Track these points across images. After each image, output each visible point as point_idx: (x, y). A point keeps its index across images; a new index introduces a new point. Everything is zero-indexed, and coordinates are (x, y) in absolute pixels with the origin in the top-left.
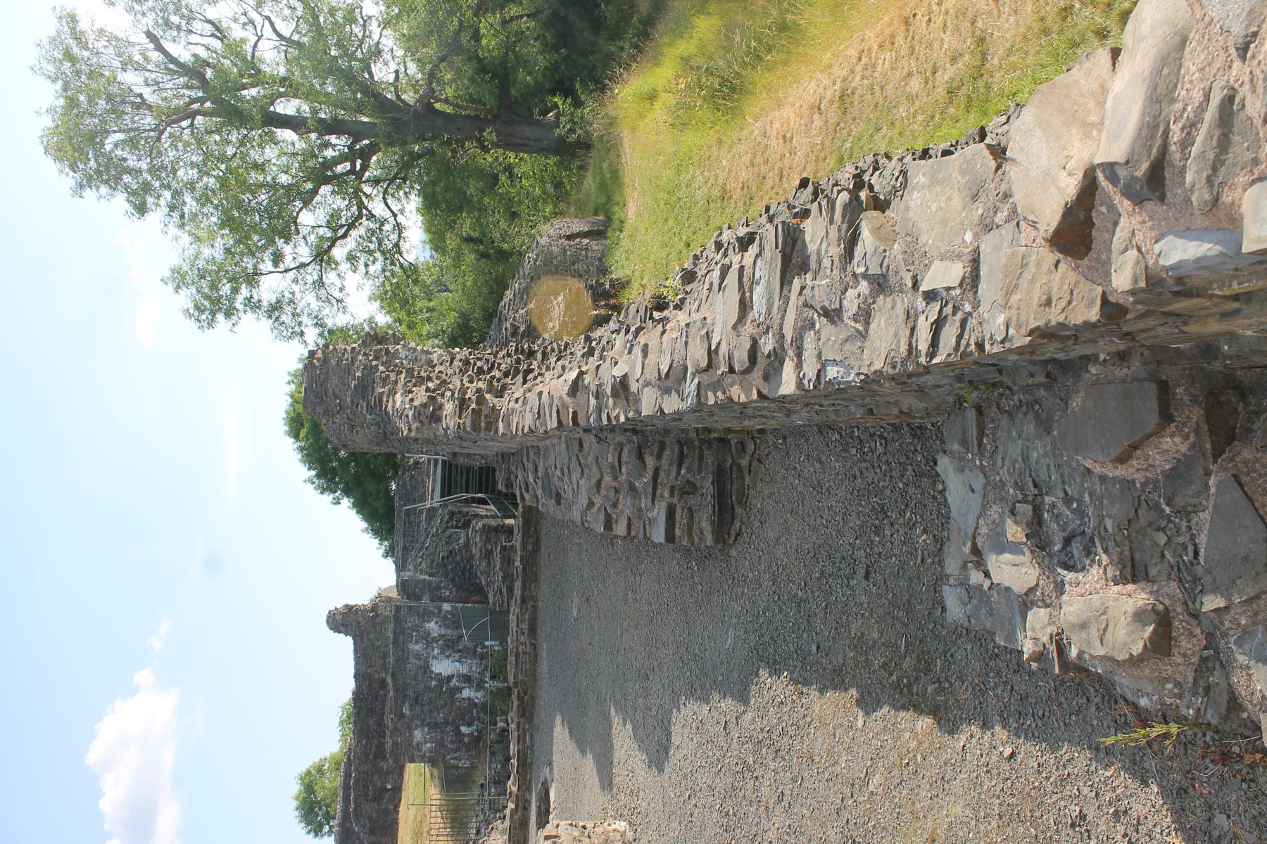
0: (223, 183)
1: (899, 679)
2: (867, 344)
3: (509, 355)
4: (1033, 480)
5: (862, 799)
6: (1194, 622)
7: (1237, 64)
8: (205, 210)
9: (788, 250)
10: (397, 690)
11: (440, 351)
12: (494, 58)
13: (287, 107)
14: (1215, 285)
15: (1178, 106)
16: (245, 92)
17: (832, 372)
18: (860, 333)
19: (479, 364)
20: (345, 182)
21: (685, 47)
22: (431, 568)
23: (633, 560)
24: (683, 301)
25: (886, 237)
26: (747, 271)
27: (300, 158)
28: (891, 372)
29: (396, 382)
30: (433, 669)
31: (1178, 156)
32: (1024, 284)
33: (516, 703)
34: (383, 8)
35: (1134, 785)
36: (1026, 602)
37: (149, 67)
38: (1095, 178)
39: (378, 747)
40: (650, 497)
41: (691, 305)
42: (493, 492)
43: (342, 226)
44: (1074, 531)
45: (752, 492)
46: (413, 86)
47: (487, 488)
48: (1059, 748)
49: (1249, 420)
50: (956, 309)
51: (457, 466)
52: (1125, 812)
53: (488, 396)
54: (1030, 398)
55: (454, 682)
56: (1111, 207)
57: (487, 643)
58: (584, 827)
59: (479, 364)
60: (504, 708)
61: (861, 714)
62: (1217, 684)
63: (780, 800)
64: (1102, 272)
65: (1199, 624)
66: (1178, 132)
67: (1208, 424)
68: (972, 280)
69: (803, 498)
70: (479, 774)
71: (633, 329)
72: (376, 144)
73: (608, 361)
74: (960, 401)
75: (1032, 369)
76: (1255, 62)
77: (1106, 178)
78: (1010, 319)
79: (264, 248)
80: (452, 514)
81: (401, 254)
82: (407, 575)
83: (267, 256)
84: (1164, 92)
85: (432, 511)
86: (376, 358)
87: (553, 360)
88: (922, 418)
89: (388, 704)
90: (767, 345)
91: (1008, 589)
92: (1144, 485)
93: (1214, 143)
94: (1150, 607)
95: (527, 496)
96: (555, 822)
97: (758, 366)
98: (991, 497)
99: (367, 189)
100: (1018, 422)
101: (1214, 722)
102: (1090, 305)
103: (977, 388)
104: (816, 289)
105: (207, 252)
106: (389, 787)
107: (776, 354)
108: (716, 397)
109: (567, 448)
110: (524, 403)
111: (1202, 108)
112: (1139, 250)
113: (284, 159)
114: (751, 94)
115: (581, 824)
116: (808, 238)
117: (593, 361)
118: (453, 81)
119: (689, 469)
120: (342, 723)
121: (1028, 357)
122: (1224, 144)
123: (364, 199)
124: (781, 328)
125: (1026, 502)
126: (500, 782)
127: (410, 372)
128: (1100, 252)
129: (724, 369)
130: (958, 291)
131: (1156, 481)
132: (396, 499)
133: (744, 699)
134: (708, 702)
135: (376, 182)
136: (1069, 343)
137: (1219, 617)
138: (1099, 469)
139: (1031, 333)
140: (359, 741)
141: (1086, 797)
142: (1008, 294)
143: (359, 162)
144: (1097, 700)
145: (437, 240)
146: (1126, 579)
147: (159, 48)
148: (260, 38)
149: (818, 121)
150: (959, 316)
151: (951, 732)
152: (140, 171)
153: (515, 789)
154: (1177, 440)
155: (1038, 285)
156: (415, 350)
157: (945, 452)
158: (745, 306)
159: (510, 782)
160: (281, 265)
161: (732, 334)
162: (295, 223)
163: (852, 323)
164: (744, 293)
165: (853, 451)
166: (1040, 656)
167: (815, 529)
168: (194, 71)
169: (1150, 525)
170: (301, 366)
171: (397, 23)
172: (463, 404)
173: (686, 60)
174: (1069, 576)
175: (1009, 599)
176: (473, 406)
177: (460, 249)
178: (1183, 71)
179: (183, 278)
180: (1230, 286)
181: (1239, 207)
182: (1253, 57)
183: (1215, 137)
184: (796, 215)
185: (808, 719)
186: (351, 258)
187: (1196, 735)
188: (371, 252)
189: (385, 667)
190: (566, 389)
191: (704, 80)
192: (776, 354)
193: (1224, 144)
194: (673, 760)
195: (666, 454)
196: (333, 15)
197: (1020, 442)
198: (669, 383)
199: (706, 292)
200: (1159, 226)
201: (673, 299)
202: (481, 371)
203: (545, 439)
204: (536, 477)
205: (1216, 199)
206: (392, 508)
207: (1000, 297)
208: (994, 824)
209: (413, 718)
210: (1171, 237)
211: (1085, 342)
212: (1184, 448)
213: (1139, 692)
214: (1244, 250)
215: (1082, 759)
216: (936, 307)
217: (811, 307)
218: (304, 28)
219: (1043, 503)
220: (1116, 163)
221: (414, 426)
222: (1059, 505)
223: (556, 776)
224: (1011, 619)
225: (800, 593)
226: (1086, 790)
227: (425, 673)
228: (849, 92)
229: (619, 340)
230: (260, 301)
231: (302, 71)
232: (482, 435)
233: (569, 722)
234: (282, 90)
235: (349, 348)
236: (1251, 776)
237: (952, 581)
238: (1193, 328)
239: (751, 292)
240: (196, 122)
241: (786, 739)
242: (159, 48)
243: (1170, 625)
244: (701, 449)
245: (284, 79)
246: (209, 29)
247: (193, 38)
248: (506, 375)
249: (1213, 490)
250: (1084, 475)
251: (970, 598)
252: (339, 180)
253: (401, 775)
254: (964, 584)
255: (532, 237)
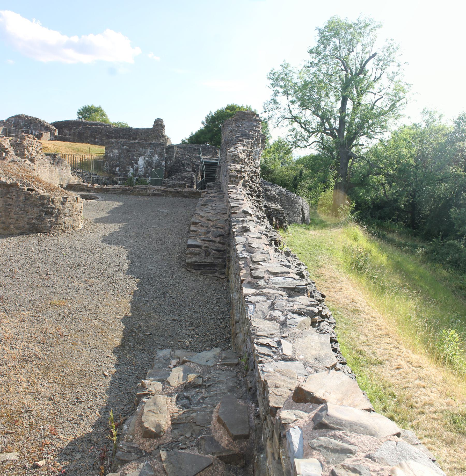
0: (321, 82)
1: (135, 332)
2: (261, 320)
3: (258, 188)
4: (211, 385)
5: (89, 317)
6: (156, 447)
7: (364, 455)
8: (311, 75)
9: (296, 290)
10: (133, 144)
11: (259, 163)
12: (369, 180)
13: (349, 104)
14: (283, 450)
15: (349, 434)
16: (355, 89)
17: (251, 307)
18: (265, 317)
19: (254, 177)
20: (322, 127)
21: (375, 251)
22: (178, 158)
23: (181, 232)
24: (278, 252)
25: (301, 326)
26: (288, 275)
27: (330, 110)
28: (251, 329)
29: (248, 147)
30: (140, 158)
31: (330, 434)
32: (283, 378)
33: (128, 188)
34: (387, 139)
35: (92, 422)
36: (164, 381)
37: (363, 54)
38: (322, 403)
39: (111, 136)
40: (204, 239)
41: (276, 254)
42: (206, 181)
43: (305, 126)
44: (192, 401)
45: (206, 277)
46: (358, 151)
47: (207, 179)
48: (107, 393)
49: (234, 469)
50: (274, 353)
51: (216, 168)
52: (82, 419)
53: (242, 181)
54: (242, 384)
55: (135, 165)
56: (311, 410)
57: (150, 178)
58: (81, 212)
59: (254, 177)
60: (126, 183)
61: (122, 317)
62: (131, 456)
63: (89, 286)
64: (288, 407)
65: (155, 449)
66: (339, 434)
67: (232, 455)
68: (285, 359)
69: (203, 296)
70: (101, 173)
71: (267, 233)
72: (336, 138)
73: (256, 225)
74: (241, 357)
75: (253, 382)
76: (364, 461)
77: (322, 407)
78: (270, 373)
79: (297, 97)
80: (198, 166)
81: (296, 148)
82: (176, 148)
83: (294, 99)
84: (354, 428)
85: (199, 158)
86: (256, 139)
87: (256, 204)
88: (233, 342)
89: (128, 141)
90: (261, 283)
91: (169, 374)
92: (209, 428)
93: (335, 447)
94: (162, 430)
95: (205, 193)
96: (83, 202)
97: (253, 280)
98: (204, 368)
99: (319, 135)
100: (233, 379)
101: (117, 454)
102: (276, 403)
103: (246, 364)
104: (282, 300)
105: (295, 76)
106: (96, 140)
107: (258, 286)
108: (242, 264)
109: (223, 209)
110: (240, 194)
111: (348, 442)
112: (296, 420)
113: (330, 104)
114: (357, 276)
115: (82, 211)
116: (301, 297)
117: (255, 219)
118: (360, 166)
119: (214, 254)
120: (120, 123)
121: (257, 380)
122: (334, 451)
123: (316, 134)
124: (267, 288)
125: (203, 382)
126: (98, 181)
127: (251, 152)
128: (295, 406)
129: (252, 267)
130: (281, 353)
131: (210, 433)
132: (204, 145)
133: (128, 273)
134: (127, 259)
135: (322, 138)
136: (263, 396)
137: (158, 457)
138: (215, 411)
139: (265, 381)
140: (113, 129)
141: (88, 404)
142: (279, 372)
143: (329, 132)
144: (125, 409)
145: (300, 161)
146: (173, 421)
147: (370, 58)
148: (375, 94)
149: (348, 301)
150: (272, 354)
151: (114, 352)
152: (325, 51)
153: (95, 187)
154: (226, 442)
155: (283, 383)
156: (260, 154)
157: (222, 351)
158: (275, 274)
159: (97, 185)
160: (291, 104)
161: (265, 270)
162: (306, 109)
163: (269, 314)
164: (280, 274)
165: (221, 316)
166: (143, 386)
167: (192, 300)
168: (362, 70)
169: (194, 430)
170: (253, 110)
171: (382, 145)
172: (239, 171)
173: (370, 251)
174: (174, 398)
175: (165, 375)
176: (239, 175)
177: (298, 170)
178: (362, 435)
179: (286, 68)
180: (283, 455)
181: (312, 457)
182: (366, 460)
183: (337, 448)
184: (311, 293)
185: (120, 297)
186: (294, 130)
187: (111, 447)
188: (296, 136)
189: (141, 140)
190: (245, 209)
191: (362, 258)
192: (258, 286)
193: (334, 451)
194: (106, 246)
195: (220, 245)
196: (384, 121)
197: (225, 380)
198: (247, 247)
199: (280, 260)
200: (305, 428)
201: (279, 248)
202: (252, 178)
203: (227, 201)
204: (212, 197)
205: (314, 449)
206: (200, 144)
207: (279, 369)
208: (79, 368)
209: (122, 150)
210: (300, 432)
211: (263, 401)
212: (223, 444)
213: (129, 425)
214: (295, 459)
215: (103, 402)
216: (275, 345)
217: (275, 299)
218: (379, 110)
219: (202, 388)
220: (327, 411)
221: (231, 154)
222: (202, 395)
223: (100, 202)
224: (157, 375)
225: (168, 294)
226: (91, 404)
227: (139, 154)
228: (359, 313)
229: (263, 229)
230: (277, 96)
231: (363, 110)
232: (228, 179)
233: (120, 207)
234: (356, 103)
235: (260, 129)
236: (95, 468)
237: (172, 353)
238: (268, 443)
239: (281, 276)
240: (343, 71)
241: (113, 288)
242: (370, 58)
243: (155, 438)
244: (222, 258)
245: (360, 104)
246: (378, 76)
247: (374, 70)
248: (251, 187)
249: (207, 456)
250: (213, 405)
251: (166, 360)
252: (323, 124)
253: (100, 145)
254: (171, 357)
255: (302, 196)
